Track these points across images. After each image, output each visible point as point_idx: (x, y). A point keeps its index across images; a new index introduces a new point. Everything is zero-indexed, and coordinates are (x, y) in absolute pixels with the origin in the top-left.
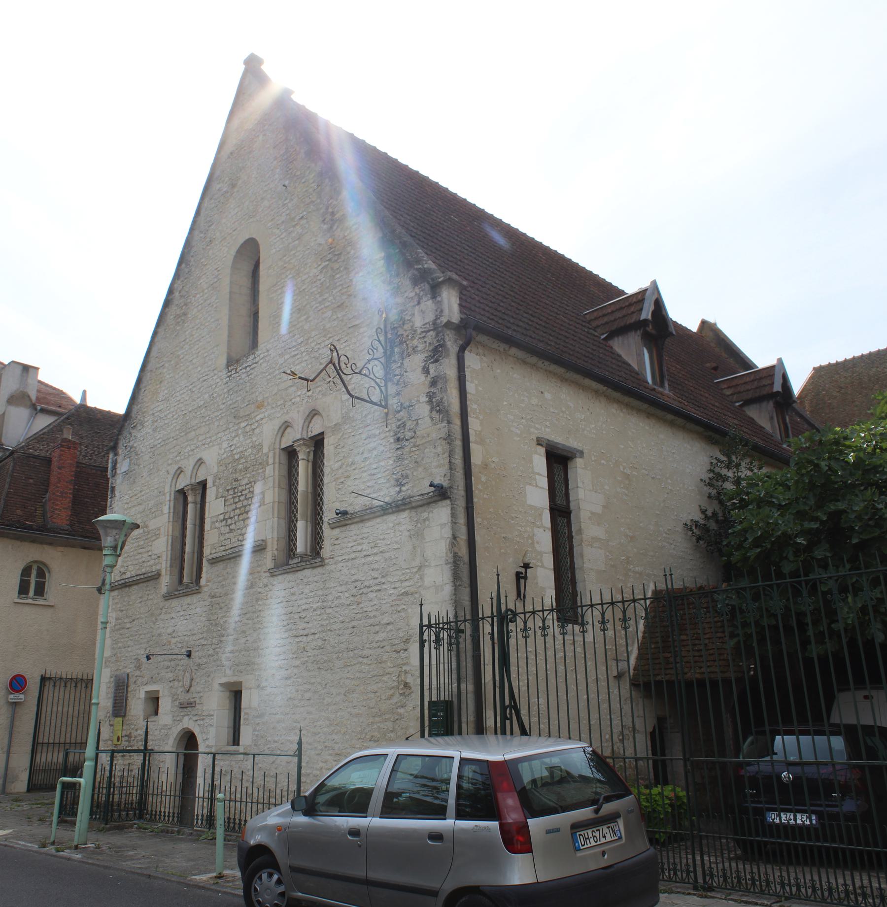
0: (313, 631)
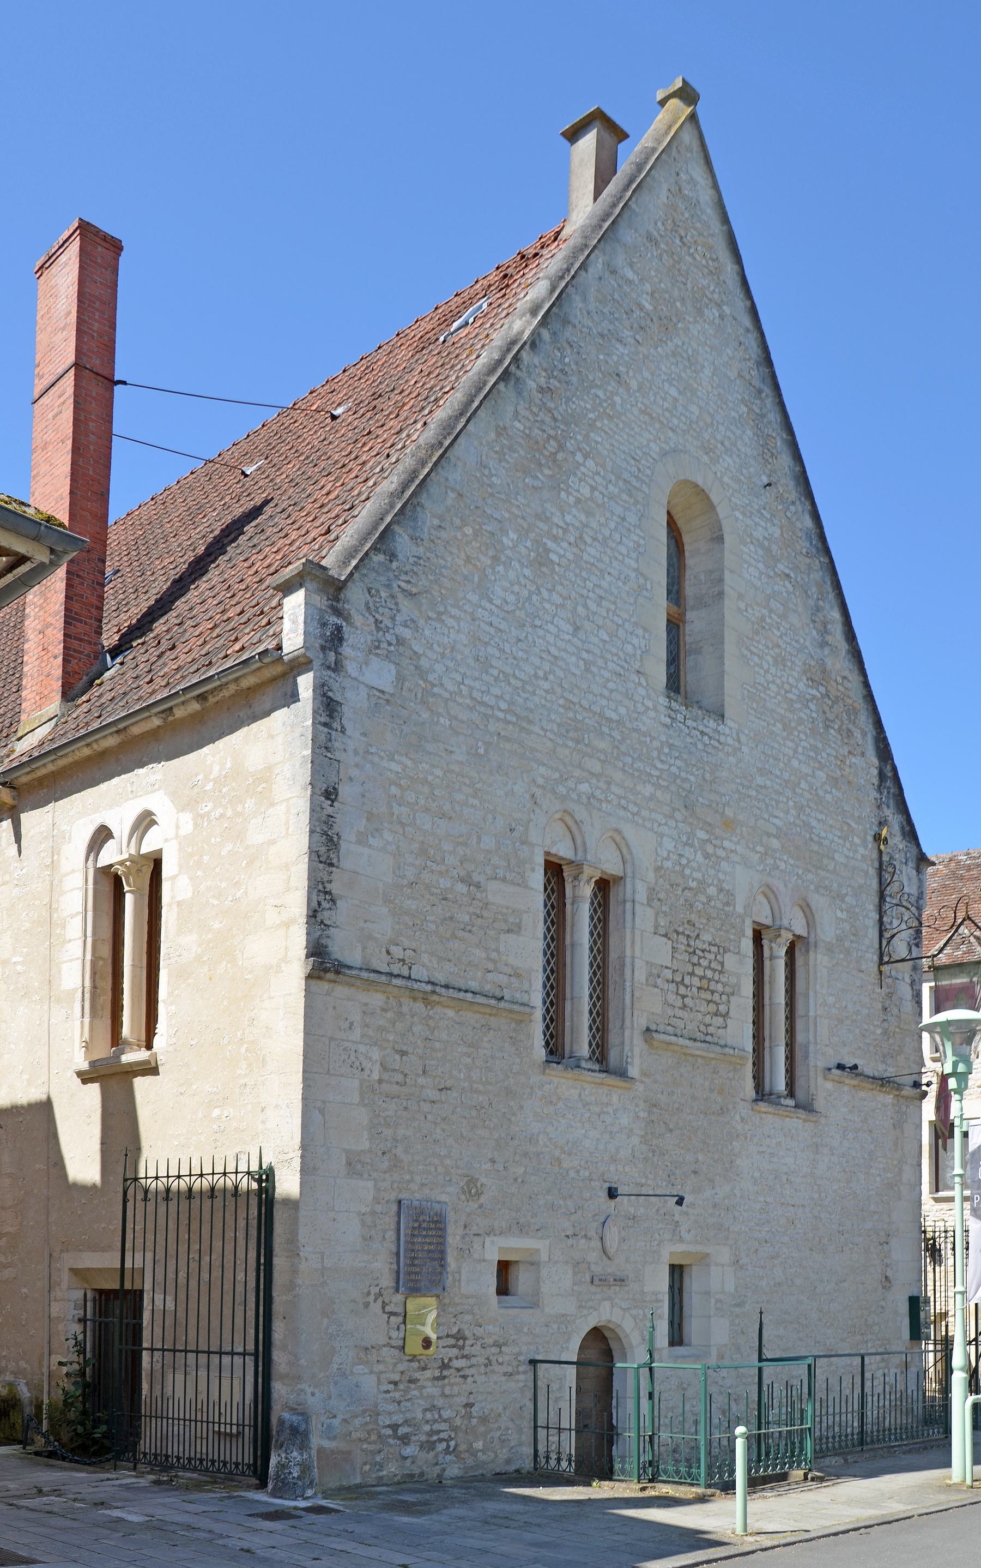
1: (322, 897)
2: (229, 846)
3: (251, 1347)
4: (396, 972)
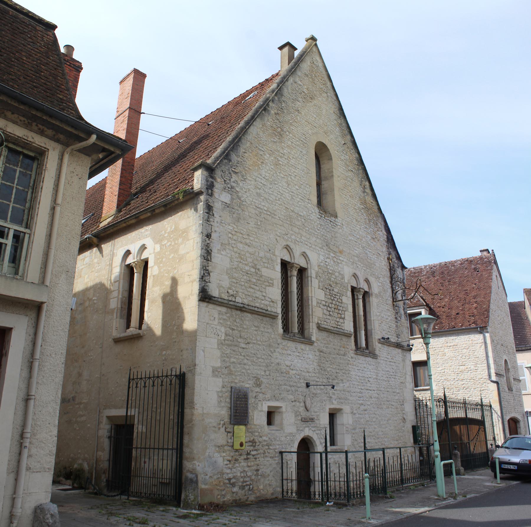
0: (374, 389)
1: (205, 272)
2: (172, 255)
3: (175, 446)
4: (230, 299)
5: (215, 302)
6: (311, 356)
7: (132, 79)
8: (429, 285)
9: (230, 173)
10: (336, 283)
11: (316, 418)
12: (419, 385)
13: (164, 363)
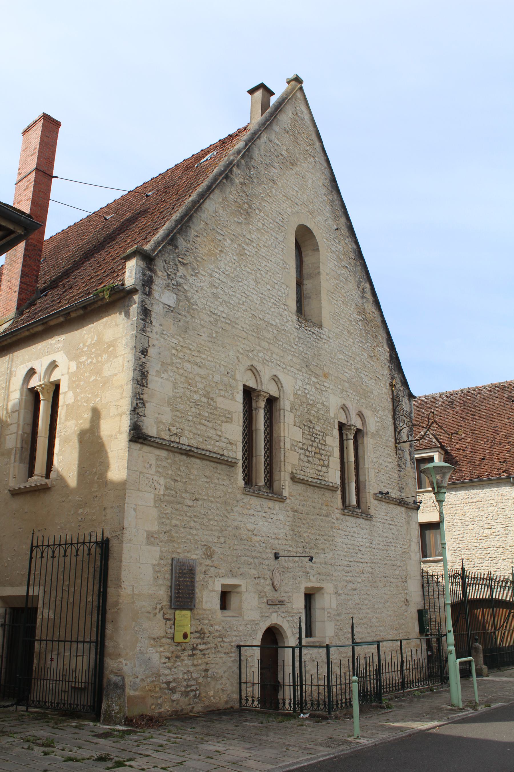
0: (366, 561)
1: (138, 402)
2: (94, 377)
3: (94, 638)
4: (173, 440)
5: (151, 444)
6: (281, 517)
7: (40, 129)
8: (445, 420)
9: (176, 265)
10: (319, 419)
11: (287, 600)
12: (428, 554)
13: (79, 526)
